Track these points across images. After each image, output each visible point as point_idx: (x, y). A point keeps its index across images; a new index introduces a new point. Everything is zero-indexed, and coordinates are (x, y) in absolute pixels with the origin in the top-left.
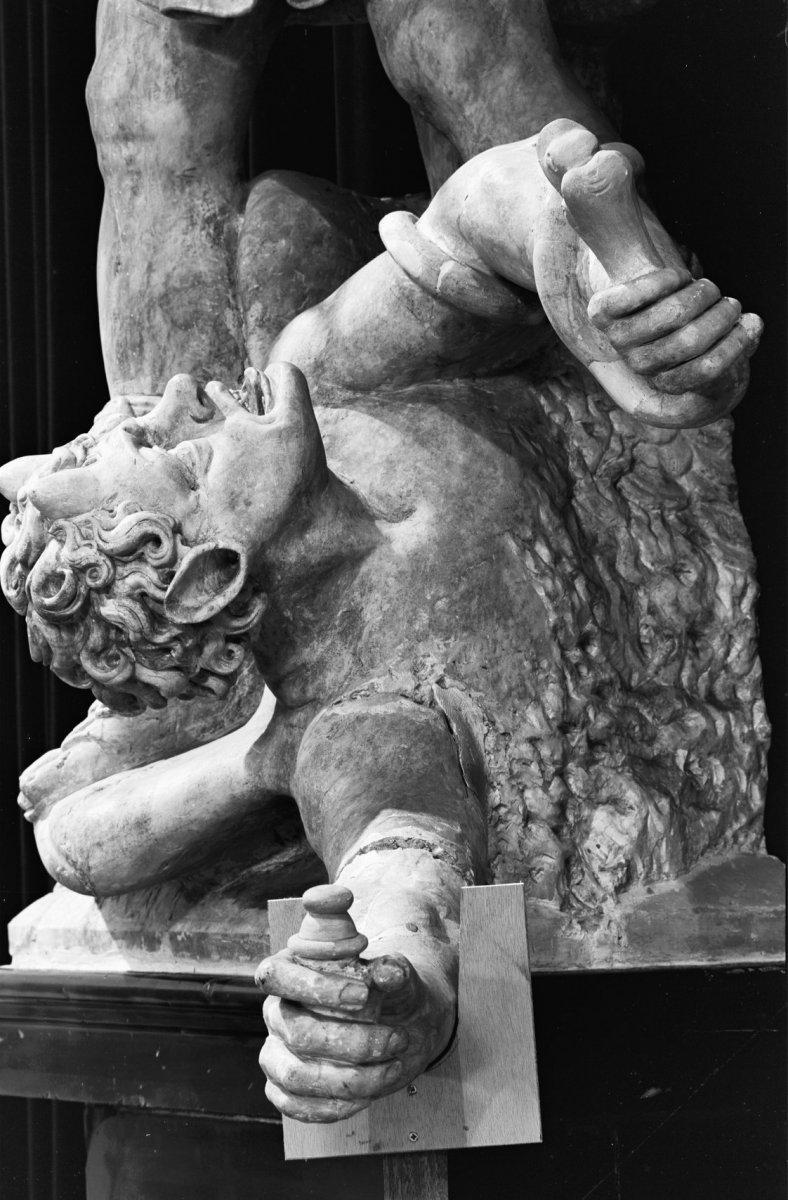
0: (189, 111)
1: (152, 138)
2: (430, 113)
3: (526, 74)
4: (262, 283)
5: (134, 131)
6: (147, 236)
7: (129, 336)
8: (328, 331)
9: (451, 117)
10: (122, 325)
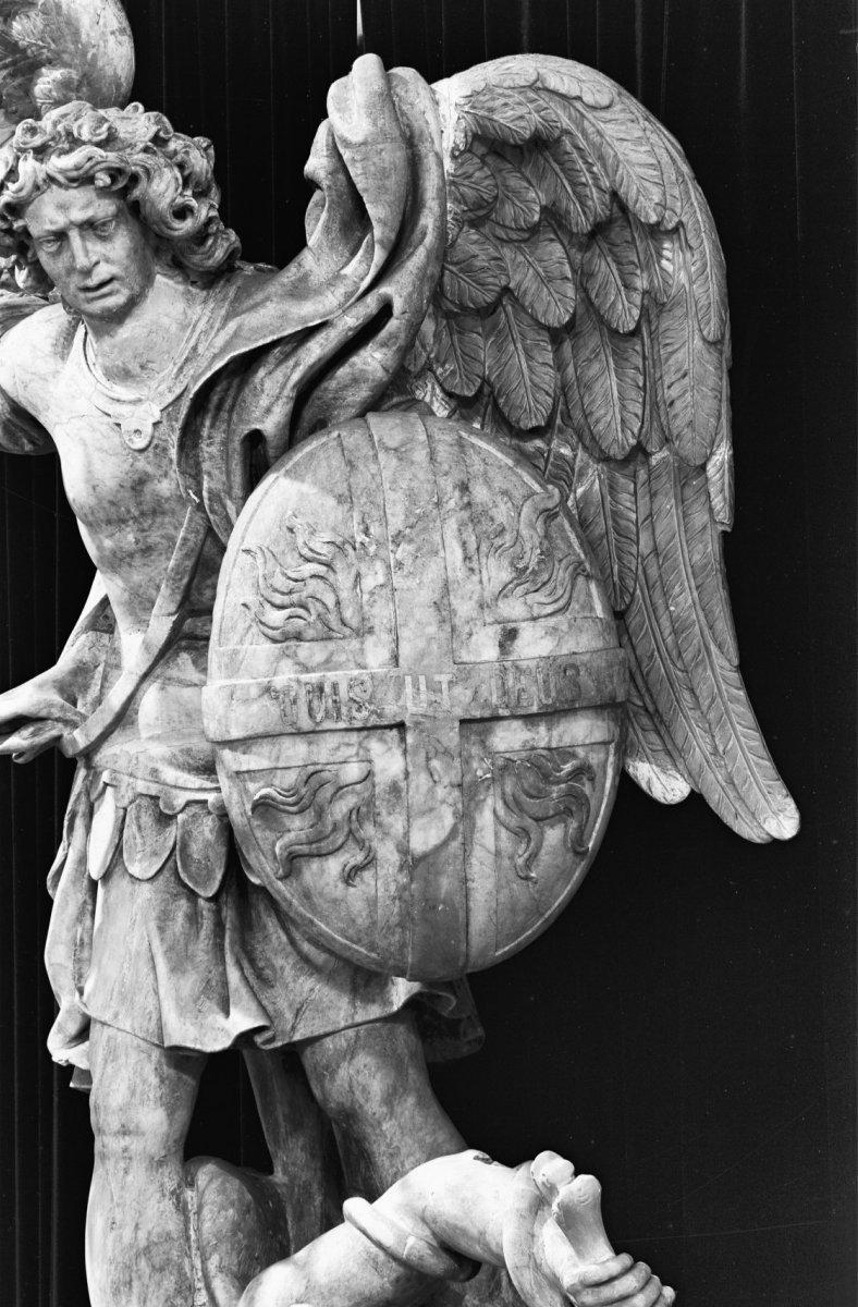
0: (168, 1115)
1: (143, 1134)
2: (351, 1126)
3: (420, 1103)
4: (219, 1240)
5: (131, 1129)
6: (134, 1204)
7: (121, 1276)
8: (306, 1280)
9: (369, 1130)
10: (116, 1269)
